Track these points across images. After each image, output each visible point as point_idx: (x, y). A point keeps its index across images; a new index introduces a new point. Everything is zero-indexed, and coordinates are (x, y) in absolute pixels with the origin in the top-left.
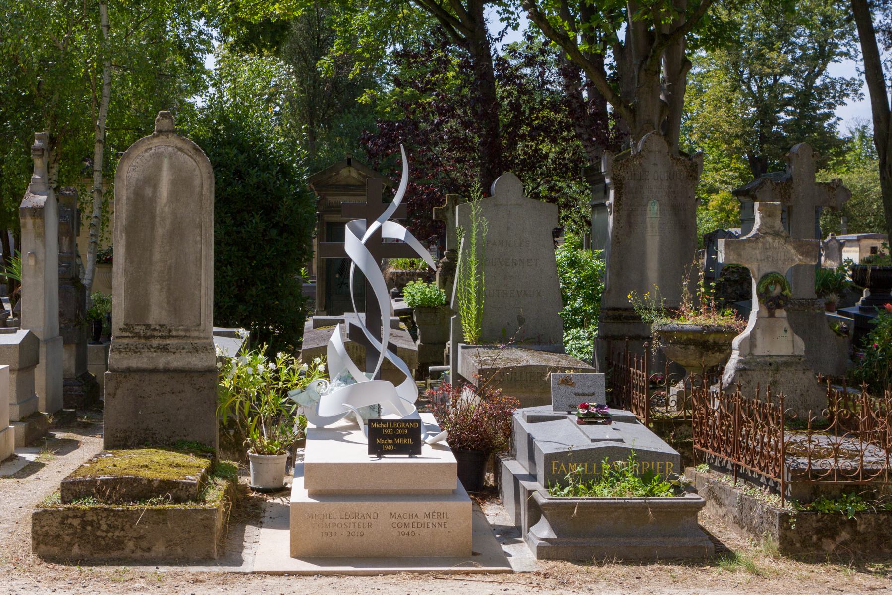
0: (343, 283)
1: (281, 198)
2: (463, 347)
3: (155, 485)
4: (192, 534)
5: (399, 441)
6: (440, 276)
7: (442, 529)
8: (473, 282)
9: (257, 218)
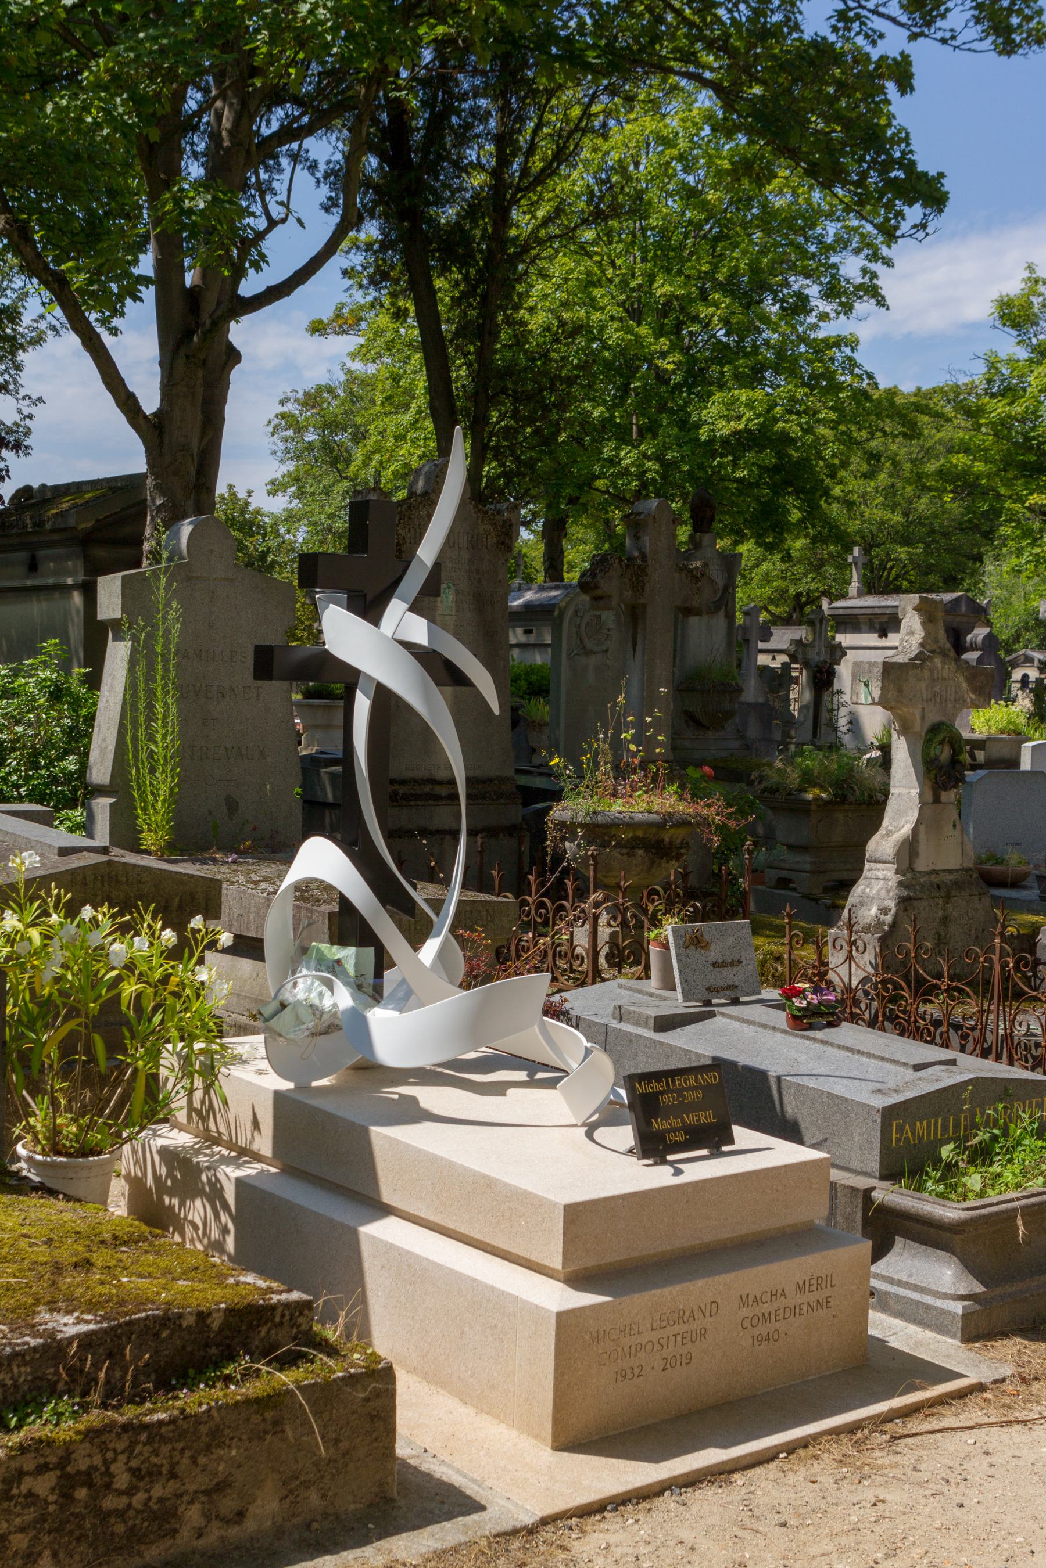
3: (216, 1325)
4: (344, 1445)
5: (690, 1119)
7: (823, 1313)
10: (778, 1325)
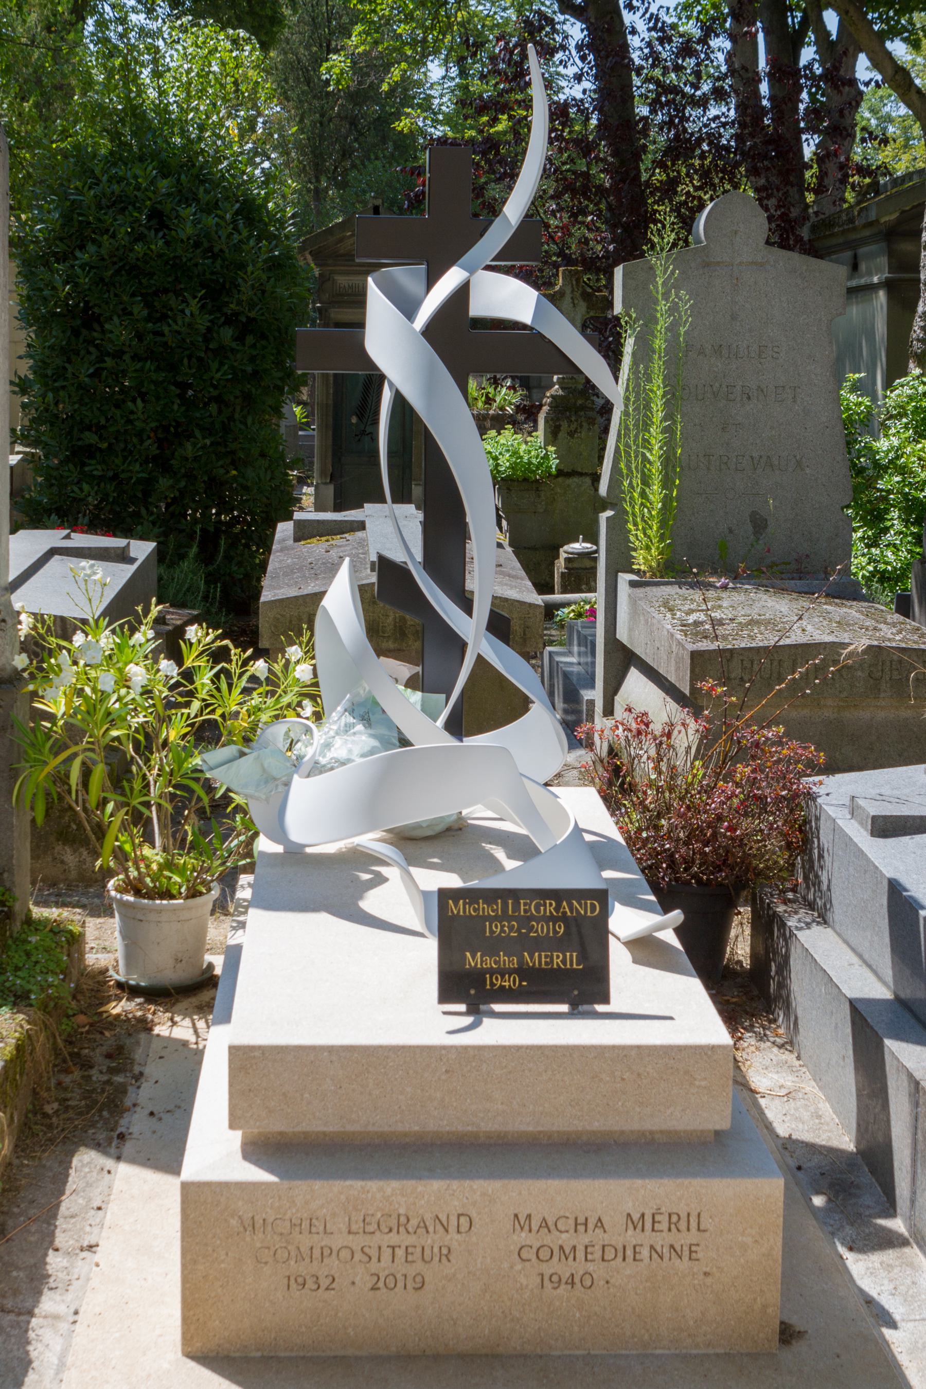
0: (363, 433)
1: (242, 266)
2: (633, 584)
5: (537, 959)
6: (546, 421)
7: (683, 1265)
8: (656, 436)
9: (194, 305)
10: (591, 1267)
